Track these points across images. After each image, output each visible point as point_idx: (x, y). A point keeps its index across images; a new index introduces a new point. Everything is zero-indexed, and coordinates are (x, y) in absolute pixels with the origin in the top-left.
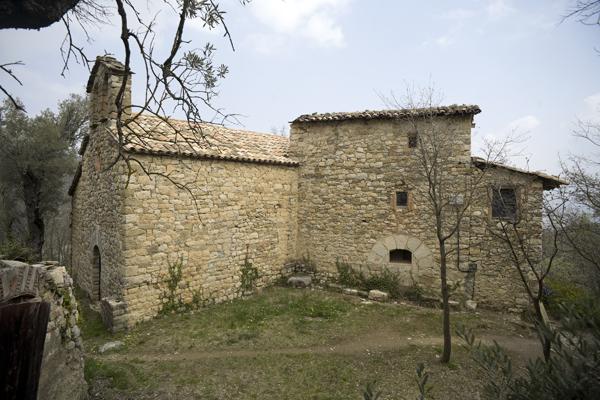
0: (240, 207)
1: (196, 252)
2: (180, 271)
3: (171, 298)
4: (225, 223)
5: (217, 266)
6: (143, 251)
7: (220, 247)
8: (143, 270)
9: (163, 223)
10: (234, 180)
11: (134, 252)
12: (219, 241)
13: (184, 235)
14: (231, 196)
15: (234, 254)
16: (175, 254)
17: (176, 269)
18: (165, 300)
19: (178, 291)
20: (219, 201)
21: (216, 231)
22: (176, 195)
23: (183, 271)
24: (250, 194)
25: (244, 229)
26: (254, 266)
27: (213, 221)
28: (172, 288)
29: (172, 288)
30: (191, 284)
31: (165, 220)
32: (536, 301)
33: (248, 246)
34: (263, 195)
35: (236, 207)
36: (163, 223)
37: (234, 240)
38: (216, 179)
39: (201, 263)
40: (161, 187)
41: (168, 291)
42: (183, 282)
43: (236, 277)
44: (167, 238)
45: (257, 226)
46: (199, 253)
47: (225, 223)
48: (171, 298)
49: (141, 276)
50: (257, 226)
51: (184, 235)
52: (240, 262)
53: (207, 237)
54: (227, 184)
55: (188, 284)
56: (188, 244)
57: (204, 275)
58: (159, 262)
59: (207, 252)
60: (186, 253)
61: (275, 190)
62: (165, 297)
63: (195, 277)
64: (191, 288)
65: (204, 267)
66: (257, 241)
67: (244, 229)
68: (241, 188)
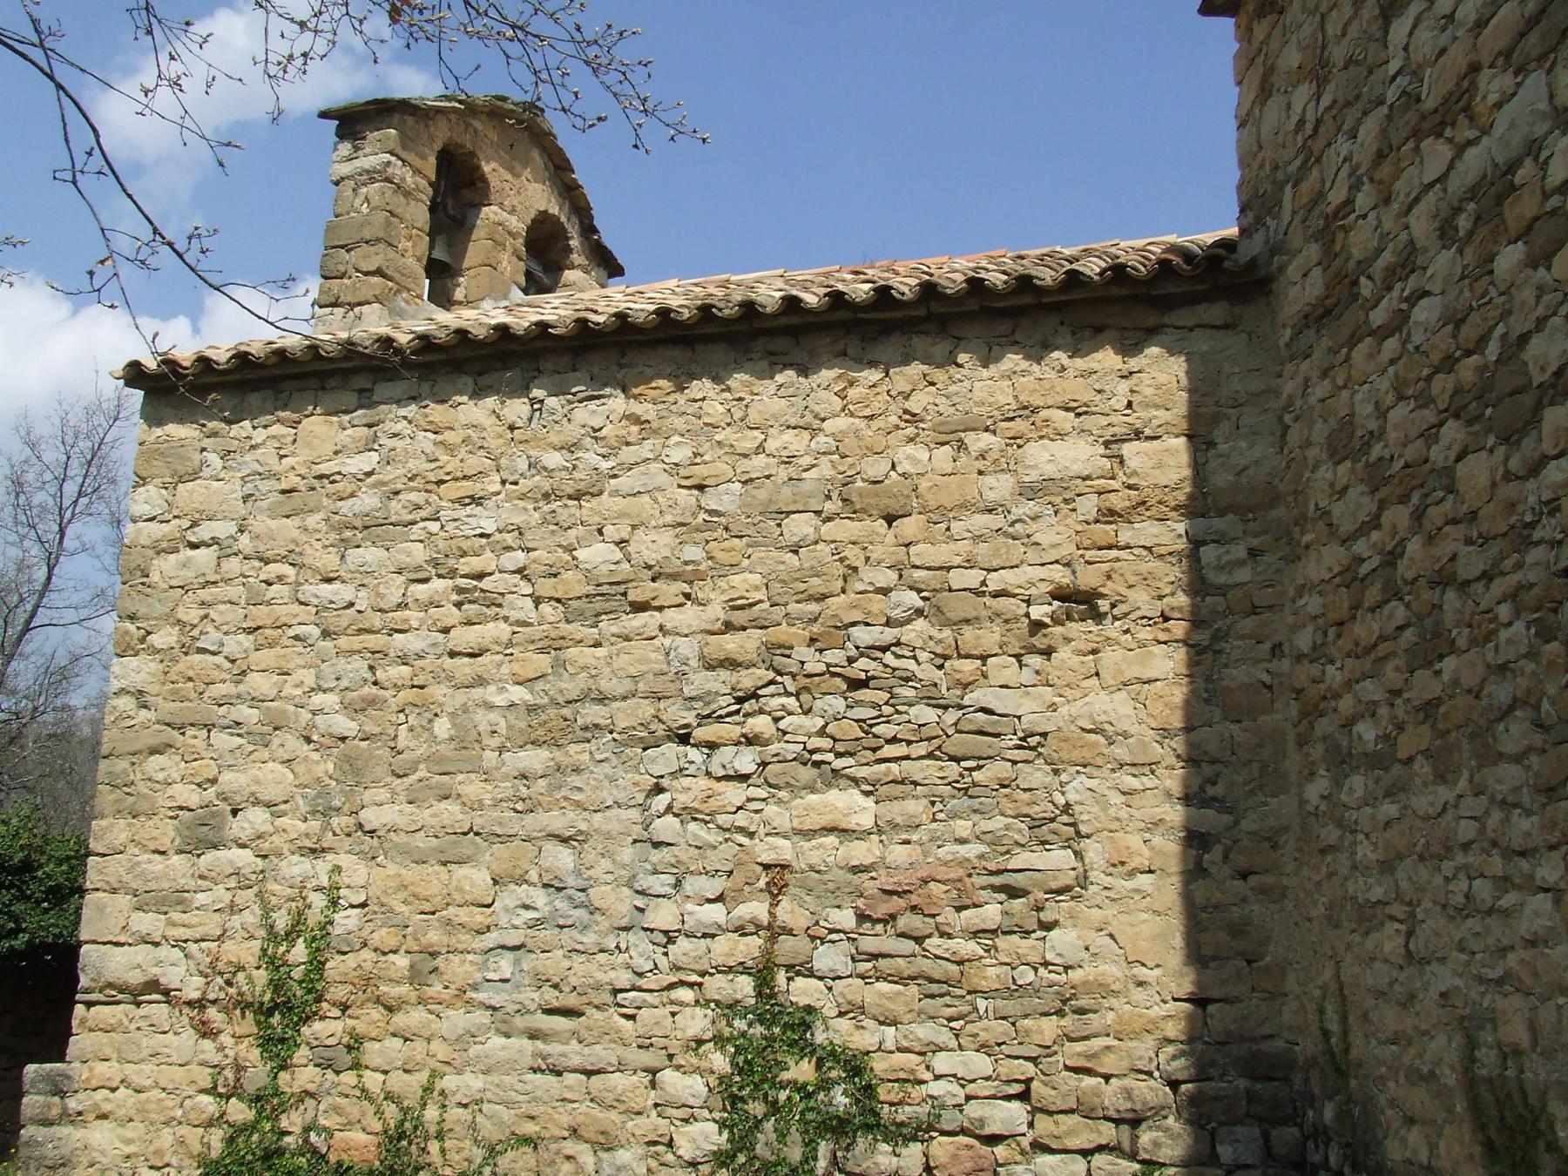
0: (716, 612)
1: (412, 873)
2: (317, 965)
3: (267, 1102)
4: (593, 713)
5: (541, 981)
6: (165, 831)
7: (562, 859)
8: (146, 922)
9: (255, 701)
10: (679, 454)
11: (1289, 1013)
12: (557, 821)
13: (353, 770)
14: (654, 546)
15: (663, 916)
16: (296, 867)
17: (300, 952)
18: (239, 1111)
19: (306, 1076)
20: (572, 584)
21: (535, 759)
22: (328, 560)
23: (336, 966)
24: (800, 526)
25: (746, 761)
26: (837, 1032)
27: (519, 694)
28: (277, 1048)
29: (277, 1048)
30: (373, 1052)
31: (259, 683)
32: (1306, 1138)
33: (778, 877)
34: (909, 526)
35: (688, 617)
36: (255, 701)
37: (666, 827)
38: (554, 459)
39: (434, 937)
40: (262, 523)
41: (258, 1073)
42: (327, 1029)
43: (685, 1086)
44: (272, 777)
45: (868, 742)
46: (432, 879)
47: (593, 713)
48: (267, 1102)
49: (142, 953)
50: (868, 742)
51: (353, 770)
52: (717, 986)
53: (473, 788)
54: (625, 482)
55: (355, 1044)
56: (370, 817)
57: (457, 1020)
58: (221, 895)
59: (475, 878)
60: (356, 871)
61: (1030, 492)
62: (235, 1091)
63: (400, 1020)
64: (373, 1080)
65: (458, 969)
66: (861, 852)
67: (746, 761)
68: (725, 498)
